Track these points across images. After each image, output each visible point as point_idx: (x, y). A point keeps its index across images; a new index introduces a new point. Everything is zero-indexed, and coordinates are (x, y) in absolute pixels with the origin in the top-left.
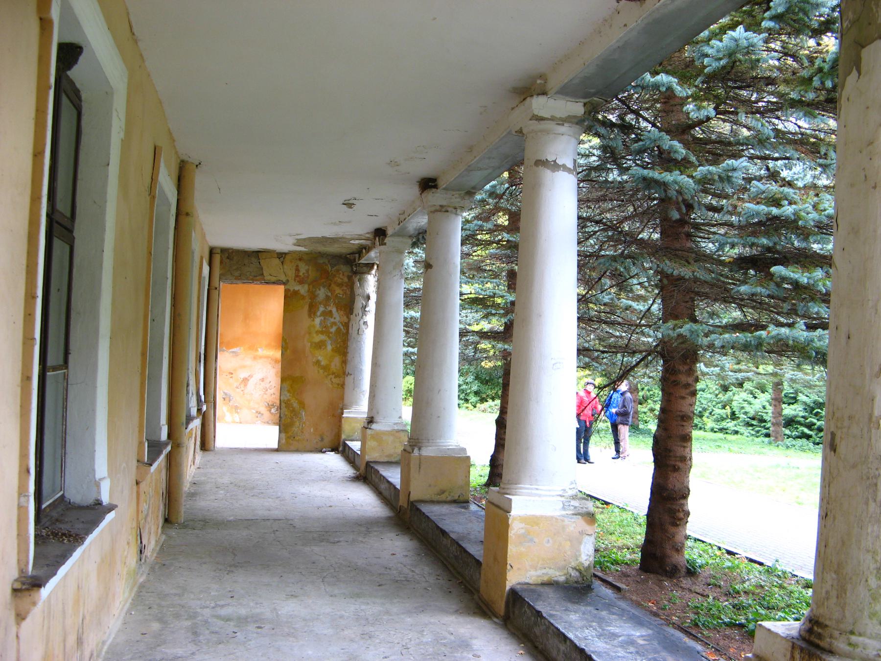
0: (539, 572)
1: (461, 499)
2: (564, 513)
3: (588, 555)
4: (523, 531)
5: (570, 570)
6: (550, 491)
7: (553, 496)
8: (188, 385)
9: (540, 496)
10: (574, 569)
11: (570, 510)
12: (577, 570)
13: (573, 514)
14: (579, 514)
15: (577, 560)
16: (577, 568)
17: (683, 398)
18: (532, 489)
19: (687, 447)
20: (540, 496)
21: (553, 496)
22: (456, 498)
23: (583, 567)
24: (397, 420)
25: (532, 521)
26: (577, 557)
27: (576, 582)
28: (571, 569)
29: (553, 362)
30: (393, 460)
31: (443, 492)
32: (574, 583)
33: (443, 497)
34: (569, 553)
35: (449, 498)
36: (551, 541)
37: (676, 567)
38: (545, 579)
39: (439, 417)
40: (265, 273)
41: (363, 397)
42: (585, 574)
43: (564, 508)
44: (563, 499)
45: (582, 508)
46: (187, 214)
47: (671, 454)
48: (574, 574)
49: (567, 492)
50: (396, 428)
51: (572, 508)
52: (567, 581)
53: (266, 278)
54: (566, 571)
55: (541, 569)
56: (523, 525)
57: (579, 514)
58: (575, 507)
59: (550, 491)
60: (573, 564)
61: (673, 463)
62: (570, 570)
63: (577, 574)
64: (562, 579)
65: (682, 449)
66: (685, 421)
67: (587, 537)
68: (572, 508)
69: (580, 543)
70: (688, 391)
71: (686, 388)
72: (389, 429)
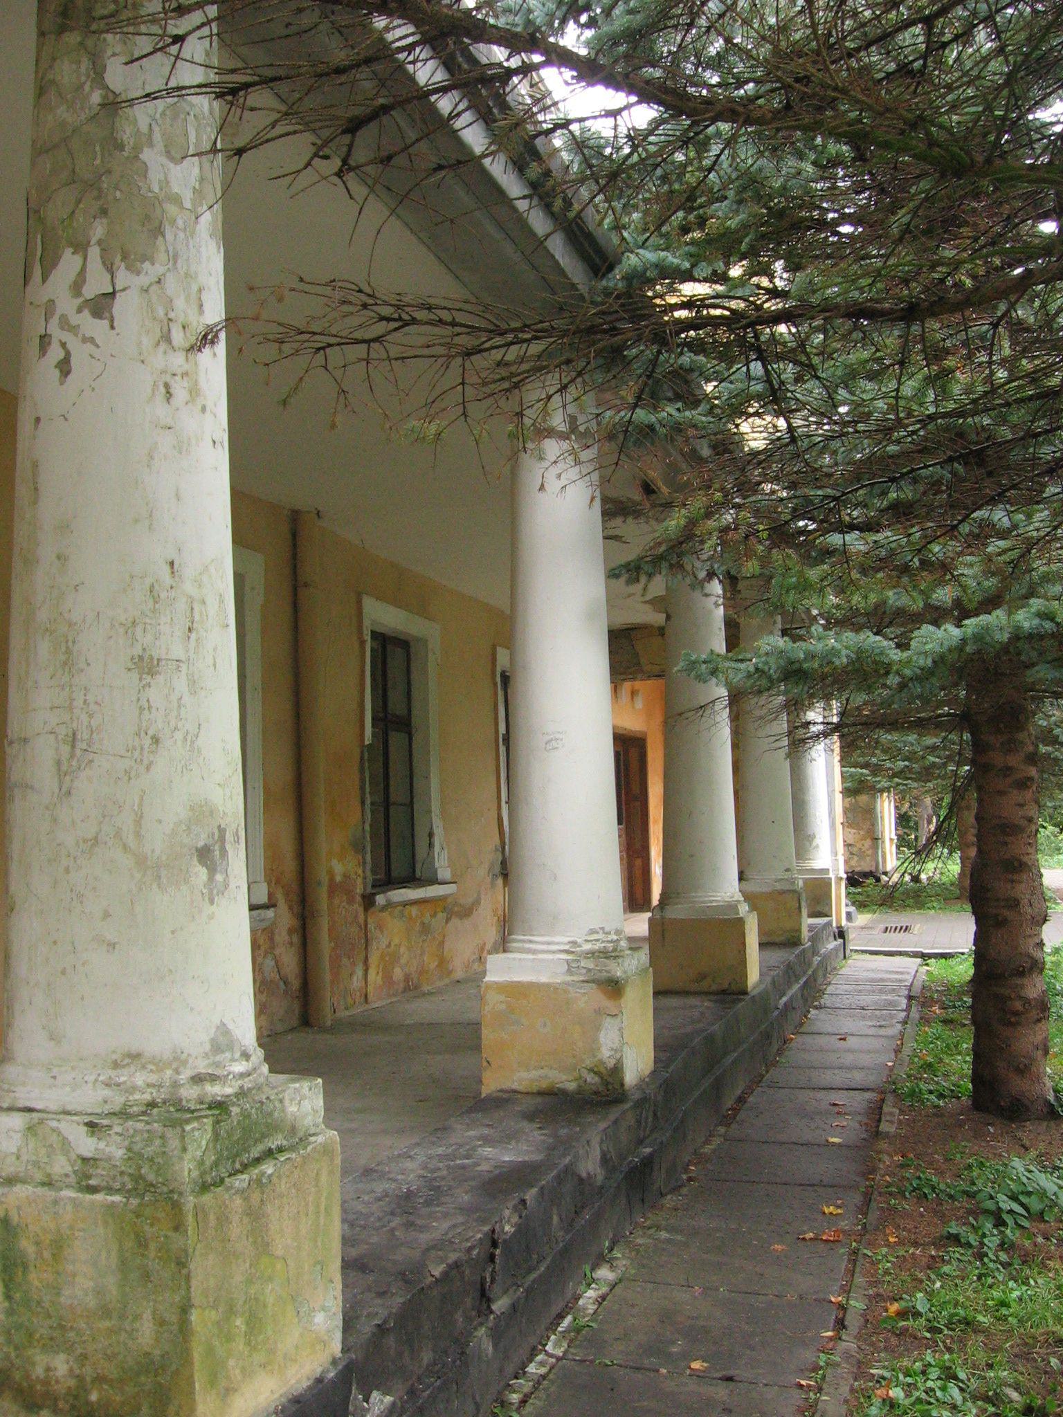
0: (535, 1074)
1: (733, 987)
2: (569, 978)
3: (612, 1049)
4: (503, 1006)
5: (585, 1073)
6: (549, 943)
7: (554, 952)
8: (431, 835)
9: (535, 952)
10: (591, 1070)
11: (581, 974)
12: (595, 1073)
13: (583, 981)
14: (593, 981)
15: (595, 1057)
16: (596, 1069)
17: (1001, 793)
18: (523, 941)
19: (1020, 882)
20: (535, 952)
21: (554, 952)
22: (726, 986)
23: (606, 1068)
24: (781, 875)
25: (517, 991)
26: (594, 1048)
27: (596, 1093)
28: (585, 1071)
29: (547, 738)
30: (778, 940)
31: (702, 977)
32: (591, 1094)
33: (705, 985)
34: (580, 1044)
35: (714, 987)
36: (549, 1024)
37: (1018, 1100)
38: (544, 1085)
39: (692, 856)
40: (643, 661)
41: (808, 844)
42: (610, 1080)
43: (570, 971)
44: (570, 957)
45: (600, 971)
46: (306, 585)
47: (989, 895)
48: (591, 1079)
49: (580, 946)
50: (779, 887)
51: (584, 971)
52: (580, 1091)
53: (645, 668)
54: (576, 1074)
55: (536, 1068)
56: (502, 998)
57: (593, 981)
58: (589, 970)
59: (549, 943)
60: (589, 1063)
61: (994, 911)
62: (585, 1073)
63: (597, 1079)
64: (572, 1086)
65: (1009, 886)
66: (1009, 835)
67: (609, 1019)
68: (584, 971)
69: (598, 1029)
70: (1009, 780)
71: (1005, 776)
72: (765, 889)
